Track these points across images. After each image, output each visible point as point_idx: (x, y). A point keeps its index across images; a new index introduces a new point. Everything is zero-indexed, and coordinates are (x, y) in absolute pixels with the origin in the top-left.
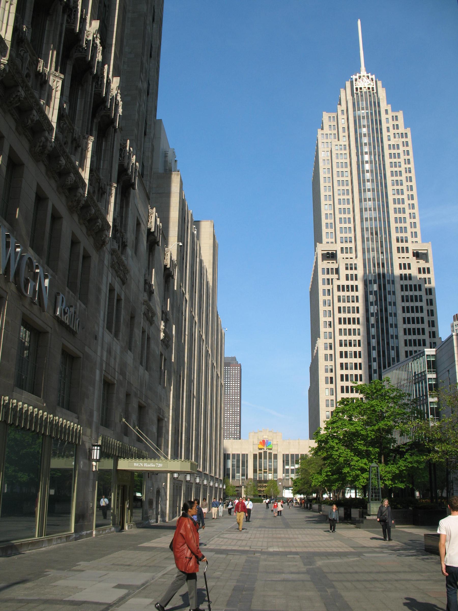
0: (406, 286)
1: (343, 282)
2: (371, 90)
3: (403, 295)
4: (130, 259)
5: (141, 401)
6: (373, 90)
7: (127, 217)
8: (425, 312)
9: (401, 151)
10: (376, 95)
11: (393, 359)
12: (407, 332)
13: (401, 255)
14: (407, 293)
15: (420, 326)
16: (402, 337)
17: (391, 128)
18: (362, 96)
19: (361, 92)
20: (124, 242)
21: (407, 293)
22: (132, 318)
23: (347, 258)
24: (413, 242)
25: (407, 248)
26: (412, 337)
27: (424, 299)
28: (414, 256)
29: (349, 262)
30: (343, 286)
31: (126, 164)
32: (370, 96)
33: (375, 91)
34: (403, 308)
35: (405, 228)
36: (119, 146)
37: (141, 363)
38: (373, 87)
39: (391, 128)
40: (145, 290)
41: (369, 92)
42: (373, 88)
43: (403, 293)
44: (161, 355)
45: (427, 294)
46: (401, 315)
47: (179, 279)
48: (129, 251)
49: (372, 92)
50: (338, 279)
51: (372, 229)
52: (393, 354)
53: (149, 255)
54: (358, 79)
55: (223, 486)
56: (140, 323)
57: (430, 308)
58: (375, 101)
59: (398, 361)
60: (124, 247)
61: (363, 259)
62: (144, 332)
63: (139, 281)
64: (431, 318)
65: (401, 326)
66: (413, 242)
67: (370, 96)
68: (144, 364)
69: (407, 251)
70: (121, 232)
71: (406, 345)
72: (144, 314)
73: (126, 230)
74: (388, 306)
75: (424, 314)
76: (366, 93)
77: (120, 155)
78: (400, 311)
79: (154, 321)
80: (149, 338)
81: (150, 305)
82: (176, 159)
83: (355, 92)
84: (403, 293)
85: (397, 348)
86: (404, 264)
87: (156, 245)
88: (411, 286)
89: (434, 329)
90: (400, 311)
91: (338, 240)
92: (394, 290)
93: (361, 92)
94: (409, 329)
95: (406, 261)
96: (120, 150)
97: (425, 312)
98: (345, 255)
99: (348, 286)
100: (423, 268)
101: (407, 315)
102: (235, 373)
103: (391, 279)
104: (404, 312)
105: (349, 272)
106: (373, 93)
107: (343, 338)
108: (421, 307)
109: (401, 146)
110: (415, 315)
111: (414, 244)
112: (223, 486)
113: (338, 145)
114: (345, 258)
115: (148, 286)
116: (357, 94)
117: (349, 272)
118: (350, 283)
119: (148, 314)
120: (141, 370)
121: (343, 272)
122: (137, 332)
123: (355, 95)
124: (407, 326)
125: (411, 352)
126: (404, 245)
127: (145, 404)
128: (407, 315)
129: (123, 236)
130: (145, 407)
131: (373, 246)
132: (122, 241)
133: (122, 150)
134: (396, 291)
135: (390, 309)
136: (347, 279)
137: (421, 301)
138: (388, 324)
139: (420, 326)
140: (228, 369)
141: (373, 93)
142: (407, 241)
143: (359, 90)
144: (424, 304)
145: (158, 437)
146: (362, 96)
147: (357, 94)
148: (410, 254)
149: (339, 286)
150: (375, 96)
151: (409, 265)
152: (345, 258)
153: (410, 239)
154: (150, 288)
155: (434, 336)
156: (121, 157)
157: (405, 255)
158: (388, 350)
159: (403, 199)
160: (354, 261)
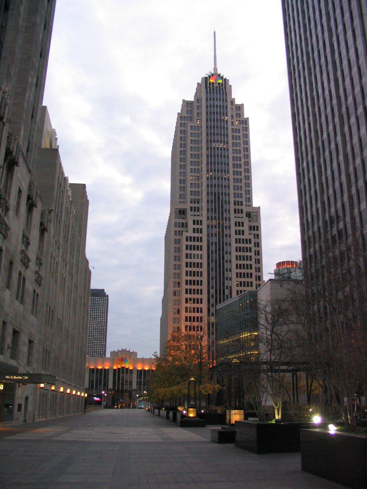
0: (240, 239)
1: (191, 234)
2: (221, 85)
3: (237, 255)
4: (11, 219)
5: (15, 328)
6: (222, 86)
7: (10, 187)
8: (253, 260)
9: (241, 134)
10: (224, 89)
11: (227, 296)
12: (238, 258)
13: (237, 215)
14: (240, 245)
15: (249, 271)
16: (234, 253)
17: (235, 116)
18: (213, 89)
19: (213, 86)
20: (7, 207)
21: (240, 245)
22: (11, 263)
23: (195, 215)
24: (246, 205)
25: (242, 210)
26: (242, 271)
27: (253, 250)
28: (247, 216)
29: (196, 218)
30: (191, 237)
31: (12, 148)
32: (220, 90)
33: (224, 87)
34: (237, 256)
35: (241, 179)
36: (7, 134)
37: (17, 298)
38: (223, 84)
39: (235, 116)
40: (23, 243)
41: (219, 87)
42: (222, 84)
43: (236, 245)
44: (34, 291)
45: (255, 246)
46: (234, 262)
47: (40, 98)
48: (11, 213)
49: (221, 87)
50: (187, 232)
51: (215, 193)
52: (227, 292)
53: (28, 214)
54: (211, 76)
55: (84, 394)
56: (18, 267)
57: (257, 257)
58: (224, 112)
59: (231, 297)
60: (7, 210)
61: (208, 263)
62: (20, 274)
63: (18, 236)
64: (258, 266)
65: (235, 271)
66: (246, 205)
67: (220, 90)
68: (20, 299)
69: (242, 213)
70: (5, 199)
71: (237, 268)
72: (21, 261)
73: (9, 197)
74: (225, 289)
75: (253, 262)
76: (217, 87)
77: (8, 141)
78: (234, 259)
79: (29, 265)
80: (24, 279)
81: (26, 254)
82: (56, 137)
83: (208, 86)
84: (236, 245)
85: (231, 287)
86: (239, 223)
87: (34, 207)
88: (243, 239)
89: (259, 274)
90: (234, 259)
91: (189, 201)
92: (231, 286)
93: (213, 86)
94: (240, 256)
95: (240, 220)
96: (8, 138)
97: (253, 260)
98: (193, 213)
99: (194, 238)
100: (253, 226)
101: (239, 262)
102: (101, 337)
103: (227, 192)
104: (237, 259)
105: (196, 227)
106: (222, 88)
107: (189, 278)
108: (251, 257)
109: (241, 131)
110: (245, 262)
111: (247, 207)
112: (84, 394)
113: (196, 215)
114: (193, 215)
115: (26, 239)
116: (210, 87)
117: (196, 227)
118: (196, 235)
119: (25, 260)
120: (17, 303)
121: (191, 226)
122: (15, 275)
123: (208, 88)
124: (239, 271)
125: (241, 291)
126: (240, 207)
127: (18, 330)
128: (239, 262)
129: (6, 202)
130: (18, 332)
131: (214, 132)
132: (6, 205)
133: (9, 137)
134: (229, 149)
135: (226, 232)
136: (194, 232)
137: (250, 251)
138: (225, 286)
139: (249, 280)
140: (93, 298)
141: (222, 88)
142: (242, 205)
143: (211, 85)
144: (252, 254)
145: (29, 355)
146: (213, 89)
147: (210, 87)
148: (244, 215)
149: (187, 237)
150: (224, 90)
151: (243, 223)
152: (193, 215)
153: (244, 203)
154: (27, 240)
155: (259, 280)
156: (8, 143)
157: (240, 215)
158: (223, 237)
159: (241, 172)
160: (199, 218)
